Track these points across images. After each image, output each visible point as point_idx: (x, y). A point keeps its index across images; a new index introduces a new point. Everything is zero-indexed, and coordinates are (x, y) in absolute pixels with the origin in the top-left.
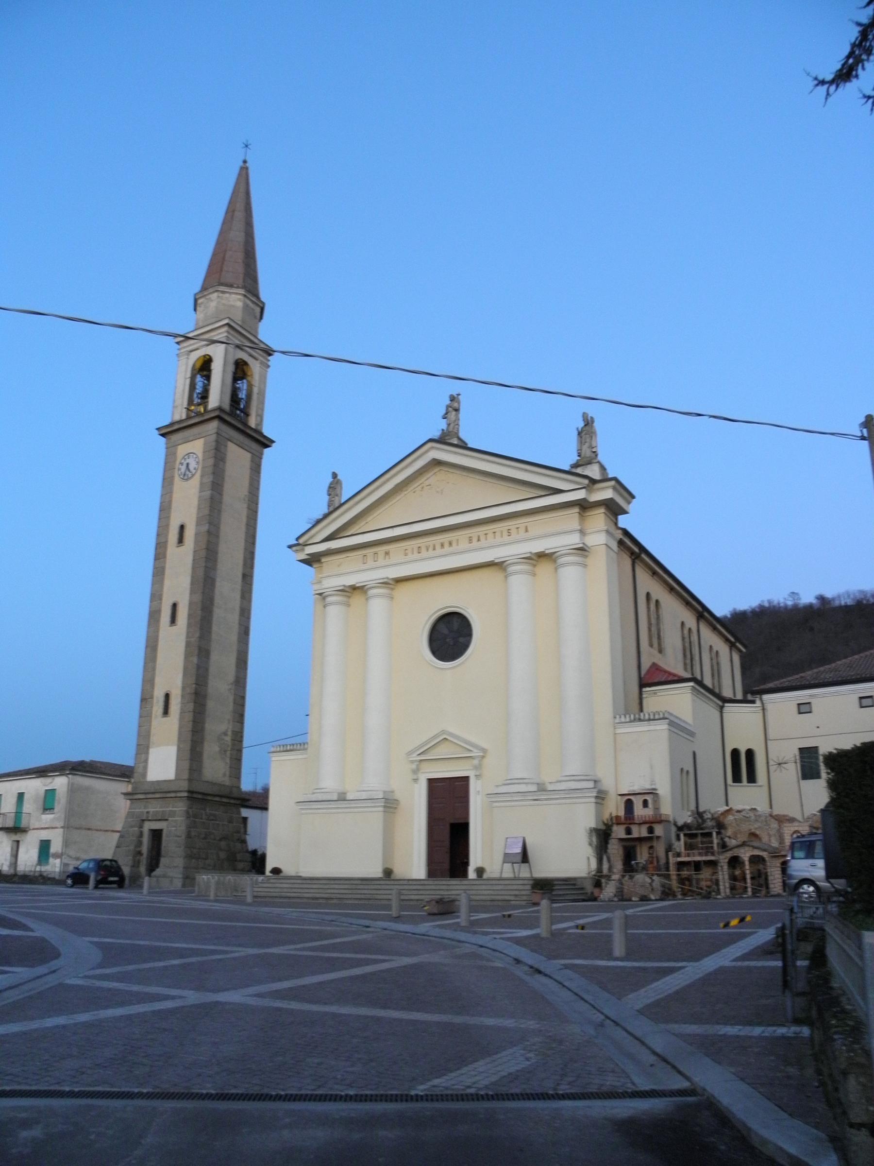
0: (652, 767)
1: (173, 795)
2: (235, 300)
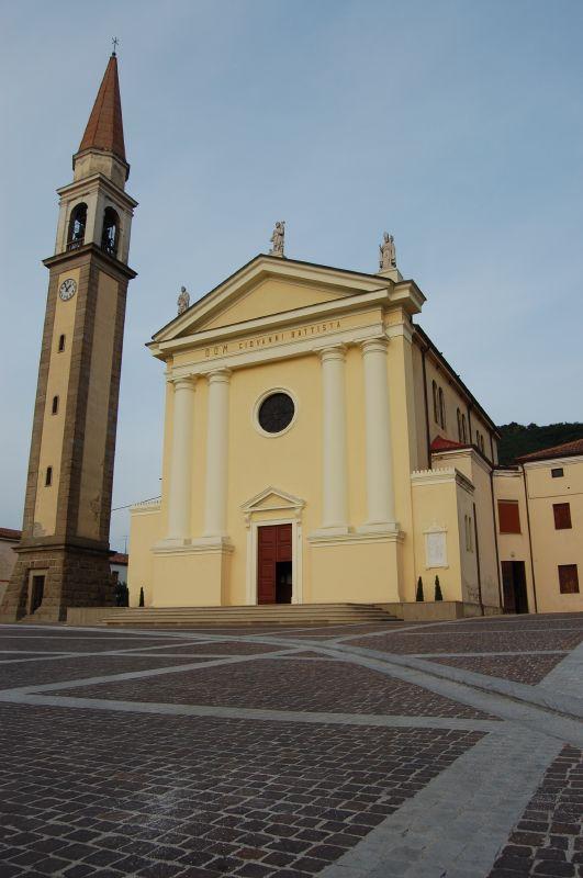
2: (106, 163)
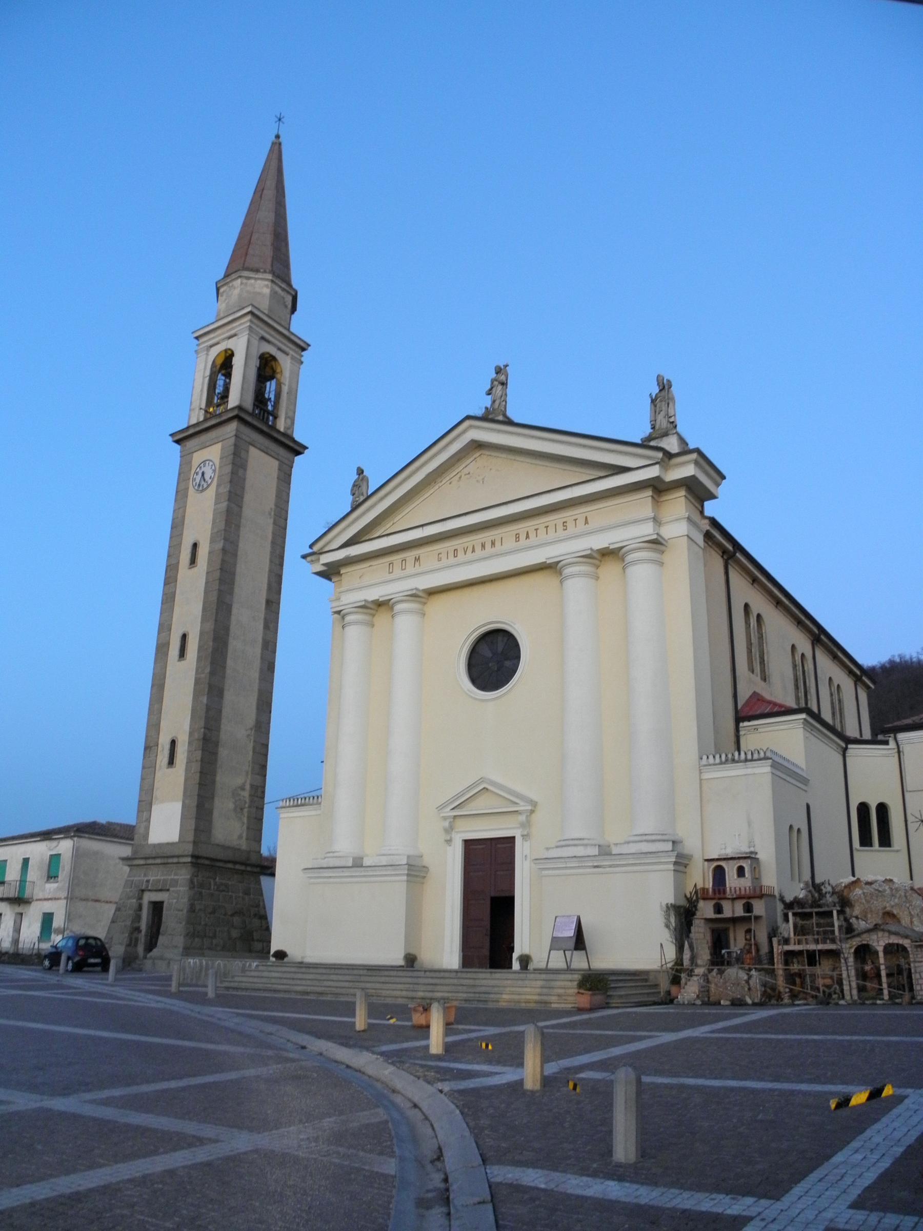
0: (749, 824)
1: (175, 860)
